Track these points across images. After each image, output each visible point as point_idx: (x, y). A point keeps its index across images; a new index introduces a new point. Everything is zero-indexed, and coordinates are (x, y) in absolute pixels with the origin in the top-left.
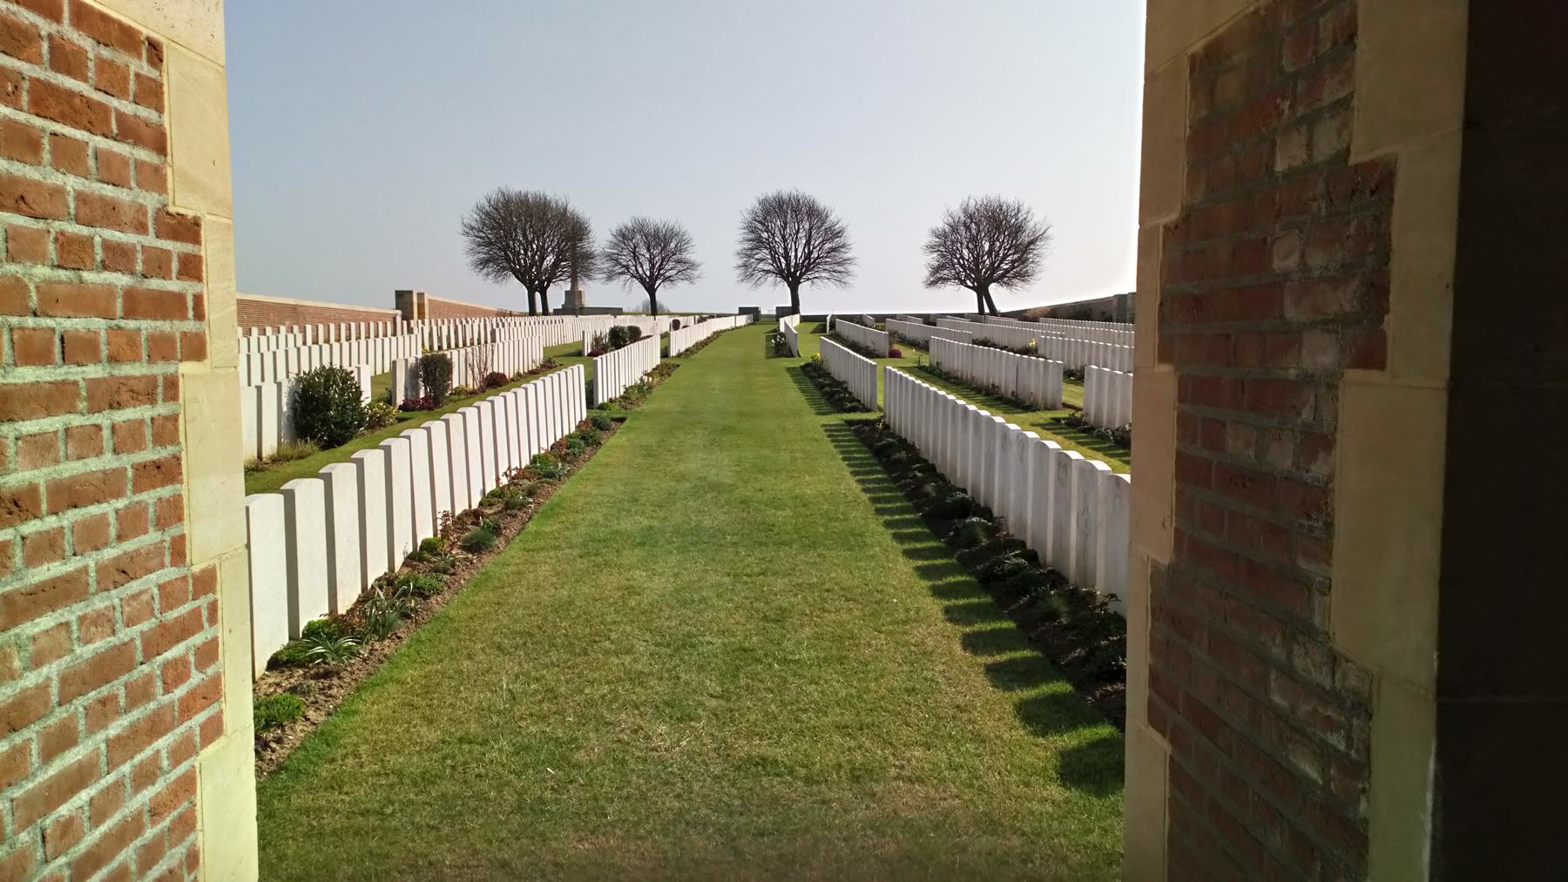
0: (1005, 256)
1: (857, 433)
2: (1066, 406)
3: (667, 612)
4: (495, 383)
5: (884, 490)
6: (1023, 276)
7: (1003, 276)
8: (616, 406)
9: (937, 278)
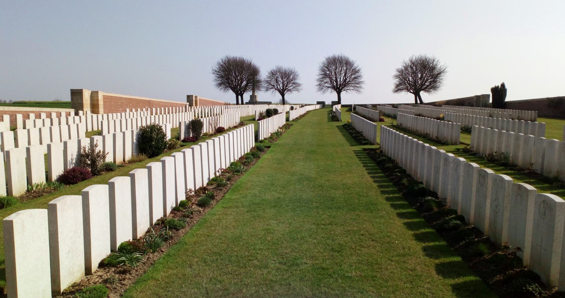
0: (428, 79)
1: (368, 154)
3: (285, 244)
4: (220, 131)
7: (426, 88)
9: (398, 89)
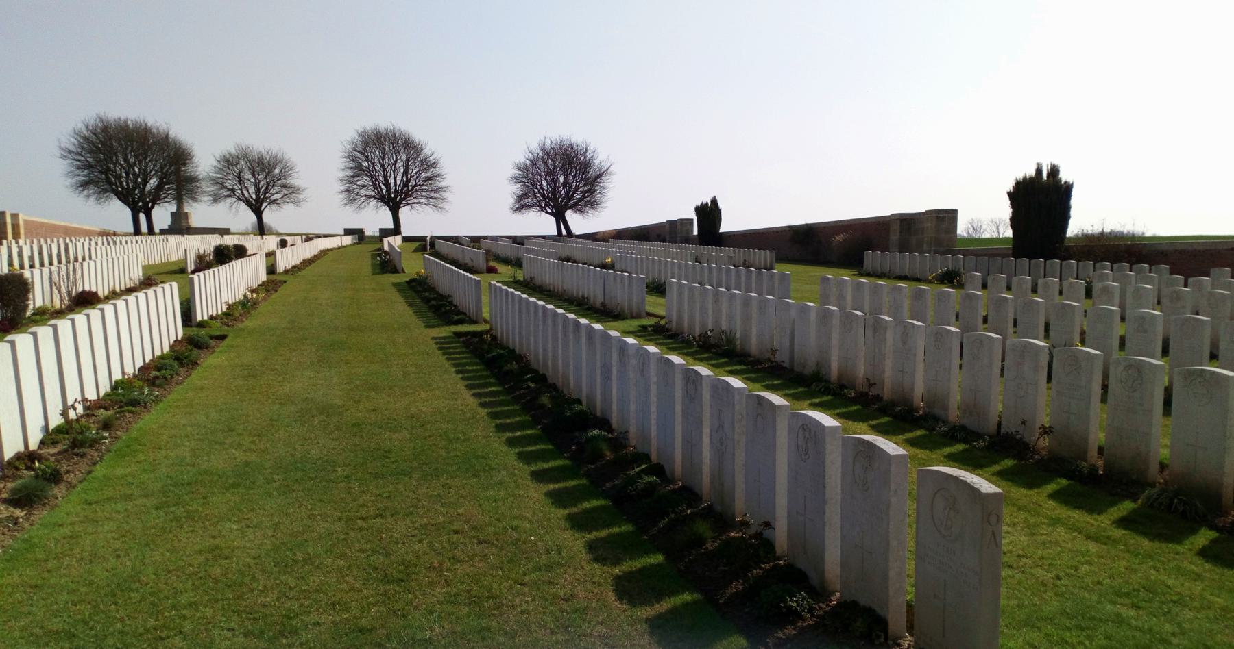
0: (577, 188)
1: (467, 344)
2: (650, 315)
4: (85, 300)
5: (500, 404)
6: (593, 205)
8: (217, 324)
9: (521, 205)
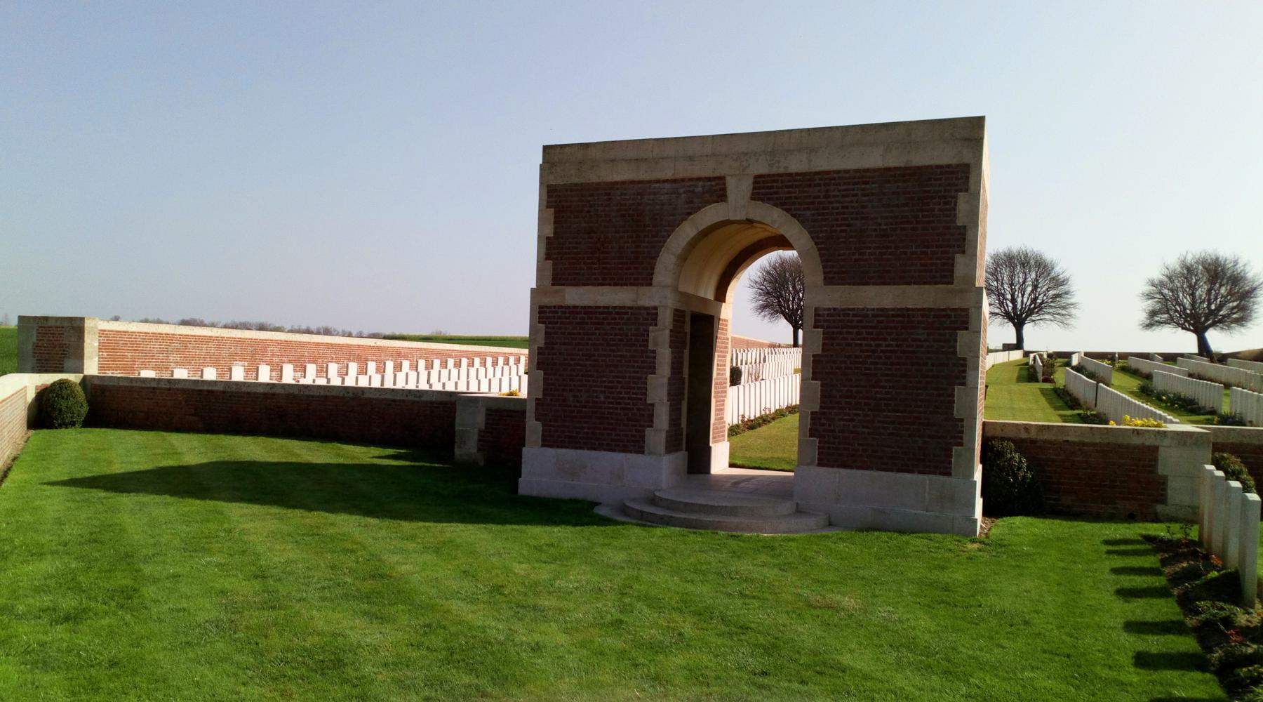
6: (1241, 321)
9: (1153, 320)
